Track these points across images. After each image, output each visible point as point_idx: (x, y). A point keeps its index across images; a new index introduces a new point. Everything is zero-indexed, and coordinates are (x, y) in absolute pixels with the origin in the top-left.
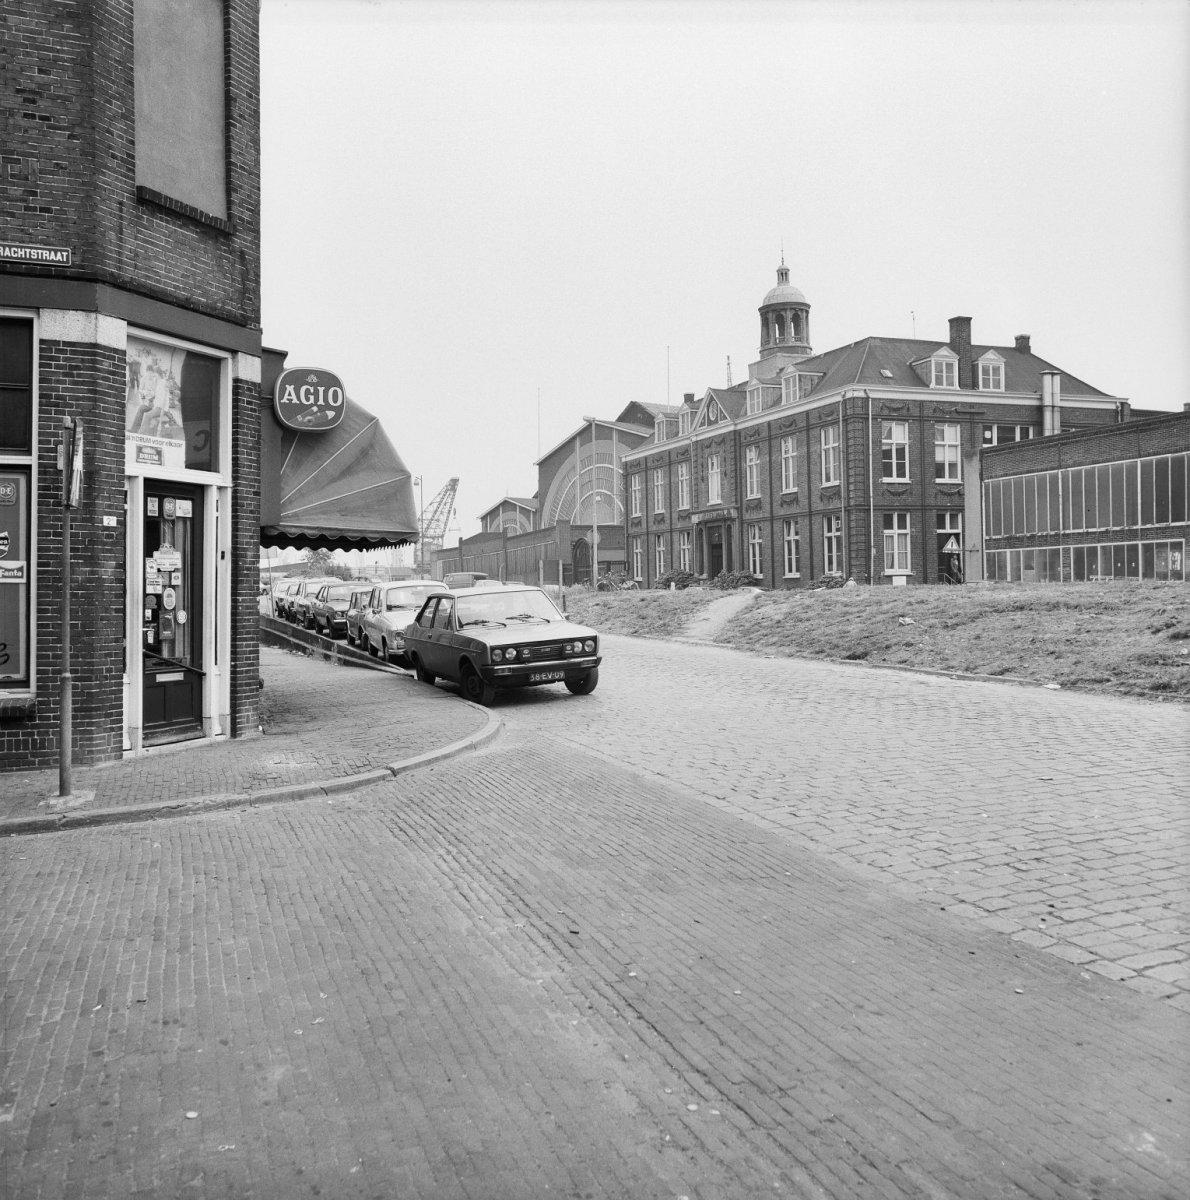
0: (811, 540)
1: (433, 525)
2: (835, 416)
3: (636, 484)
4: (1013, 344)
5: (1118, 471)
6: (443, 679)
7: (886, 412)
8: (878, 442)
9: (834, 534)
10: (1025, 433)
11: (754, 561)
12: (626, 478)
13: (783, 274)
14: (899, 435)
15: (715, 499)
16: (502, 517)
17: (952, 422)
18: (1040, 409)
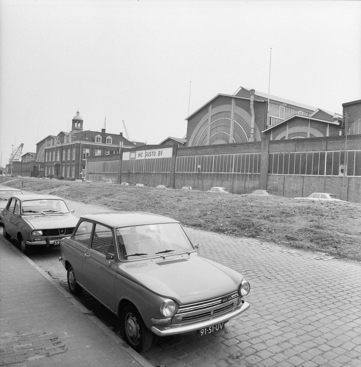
1: (16, 156)
3: (47, 153)
4: (119, 134)
5: (229, 156)
7: (84, 146)
8: (82, 152)
10: (116, 152)
12: (45, 152)
13: (78, 113)
14: (87, 151)
15: (58, 160)
16: (27, 157)
17: (99, 149)
18: (119, 148)
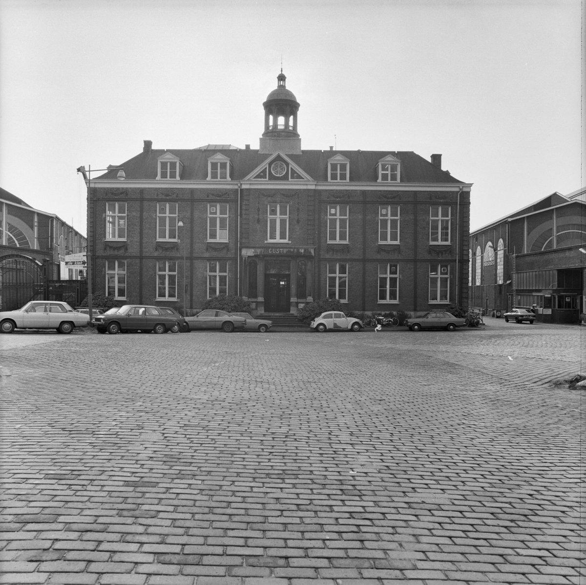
13: (282, 78)
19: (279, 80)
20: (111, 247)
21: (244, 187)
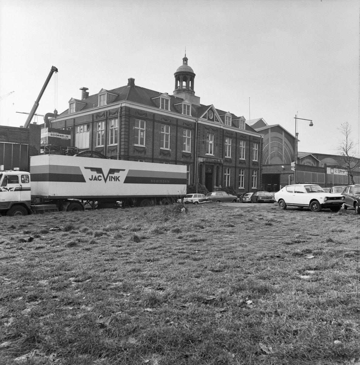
0: (249, 177)
2: (116, 114)
6: (228, 193)
9: (254, 176)
11: (242, 180)
13: (185, 60)
19: (184, 61)
20: (137, 150)
21: (199, 122)
